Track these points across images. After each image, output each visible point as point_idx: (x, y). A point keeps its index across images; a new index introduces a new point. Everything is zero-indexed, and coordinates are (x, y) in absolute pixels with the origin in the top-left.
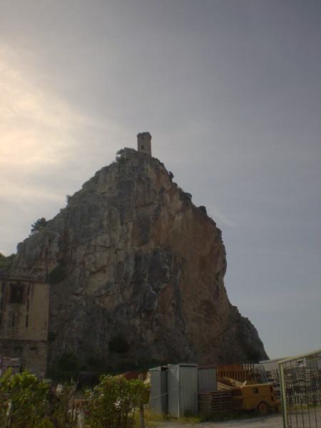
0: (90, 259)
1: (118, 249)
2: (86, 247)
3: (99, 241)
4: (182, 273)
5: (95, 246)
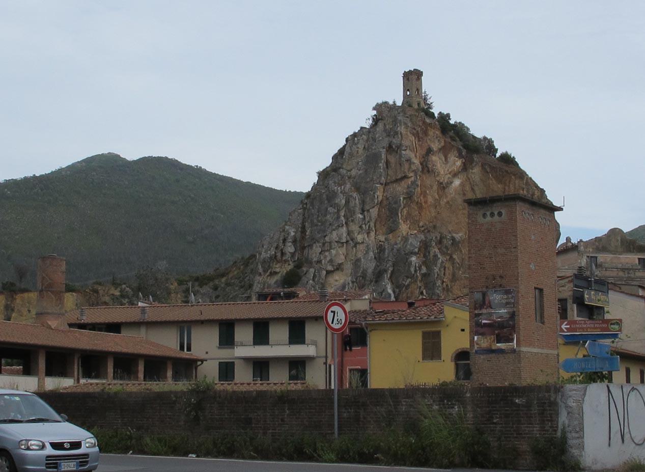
0: (325, 257)
1: (359, 243)
3: (334, 236)
4: (442, 161)
5: (330, 243)
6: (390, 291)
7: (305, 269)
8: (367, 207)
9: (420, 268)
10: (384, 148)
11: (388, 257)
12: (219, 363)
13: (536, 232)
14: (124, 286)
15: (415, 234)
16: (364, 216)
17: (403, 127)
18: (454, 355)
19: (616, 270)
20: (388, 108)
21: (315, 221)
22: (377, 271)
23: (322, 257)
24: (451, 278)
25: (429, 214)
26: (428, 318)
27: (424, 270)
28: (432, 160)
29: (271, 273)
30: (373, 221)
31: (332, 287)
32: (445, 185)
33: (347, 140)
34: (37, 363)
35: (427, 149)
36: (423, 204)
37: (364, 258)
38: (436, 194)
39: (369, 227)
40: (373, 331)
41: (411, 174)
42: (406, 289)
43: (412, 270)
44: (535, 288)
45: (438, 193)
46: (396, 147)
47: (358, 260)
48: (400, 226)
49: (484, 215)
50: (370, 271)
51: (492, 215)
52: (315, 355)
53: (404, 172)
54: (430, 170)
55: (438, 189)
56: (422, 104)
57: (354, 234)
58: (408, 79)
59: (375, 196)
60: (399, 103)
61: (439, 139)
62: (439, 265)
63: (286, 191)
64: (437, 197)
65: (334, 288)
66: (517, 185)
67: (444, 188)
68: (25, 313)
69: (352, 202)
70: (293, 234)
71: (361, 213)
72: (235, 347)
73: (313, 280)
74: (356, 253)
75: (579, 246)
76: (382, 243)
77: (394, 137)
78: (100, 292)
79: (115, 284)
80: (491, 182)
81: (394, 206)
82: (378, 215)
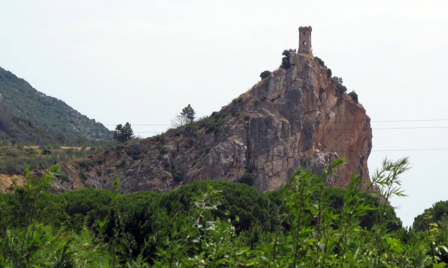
0: (268, 166)
1: (290, 157)
2: (265, 156)
5: (273, 156)
8: (294, 132)
17: (313, 73)
21: (258, 138)
29: (229, 175)
30: (298, 141)
31: (272, 188)
61: (326, 81)
69: (286, 127)
74: (288, 165)
81: (309, 131)
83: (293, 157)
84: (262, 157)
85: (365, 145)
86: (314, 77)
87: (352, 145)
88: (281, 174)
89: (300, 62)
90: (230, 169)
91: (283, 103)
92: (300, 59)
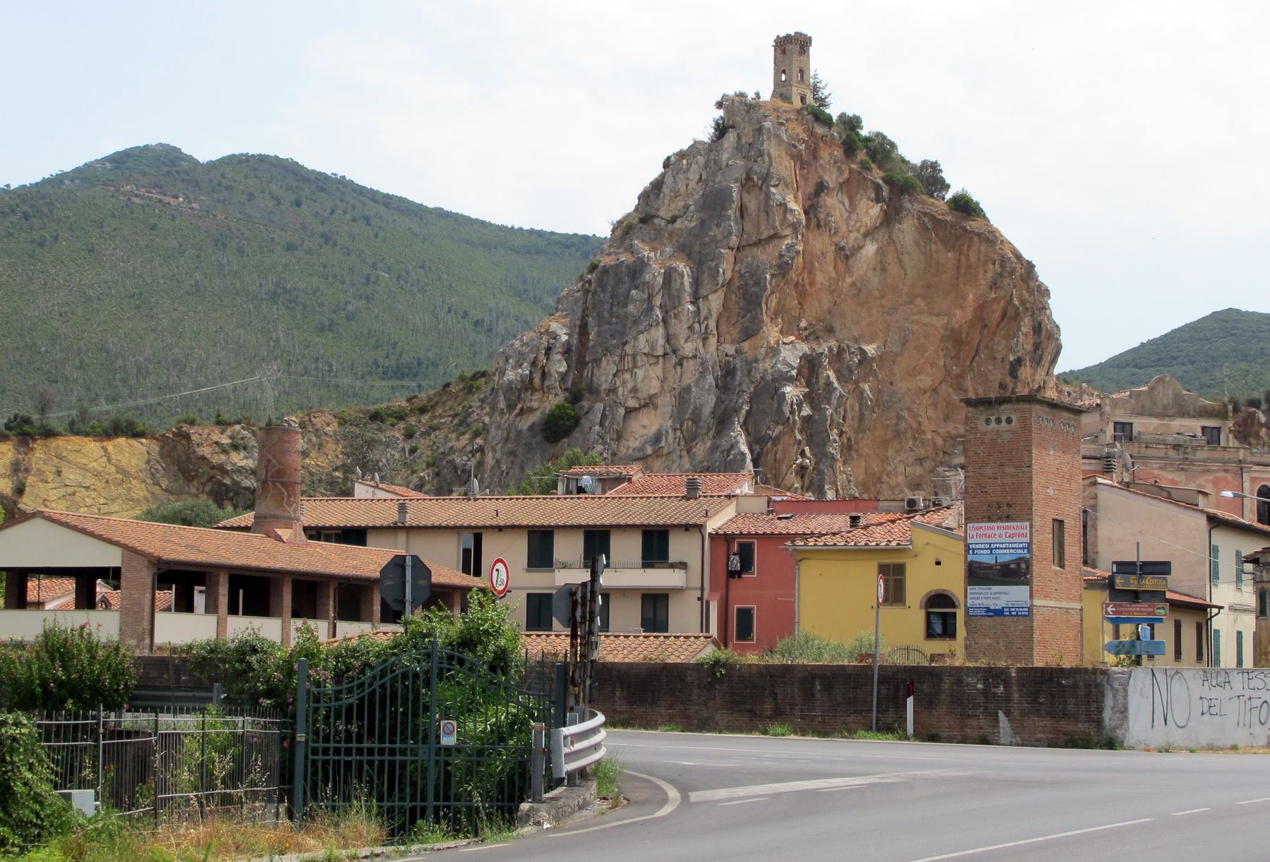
0: (624, 383)
1: (687, 358)
2: (617, 358)
5: (634, 356)
6: (744, 448)
7: (585, 404)
8: (703, 292)
9: (800, 405)
10: (736, 182)
11: (740, 384)
12: (528, 594)
13: (1056, 443)
14: (237, 427)
15: (792, 342)
16: (698, 308)
17: (773, 142)
18: (925, 600)
19: (1163, 447)
20: (746, 104)
21: (606, 315)
22: (719, 412)
23: (618, 383)
24: (856, 425)
25: (817, 305)
26: (887, 545)
27: (806, 411)
28: (825, 205)
29: (522, 409)
30: (715, 316)
31: (636, 439)
32: (848, 253)
33: (667, 164)
34: (281, 596)
35: (817, 184)
36: (808, 287)
37: (697, 386)
38: (832, 268)
39: (707, 328)
40: (804, 561)
41: (788, 231)
42: (775, 444)
43: (787, 410)
44: (1053, 520)
45: (835, 267)
46: (758, 179)
47: (687, 389)
48: (765, 328)
49: (988, 421)
50: (707, 410)
51: (999, 421)
52: (685, 586)
53: (774, 228)
54: (822, 223)
55: (835, 260)
56: (810, 100)
57: (679, 341)
58: (784, 52)
59: (718, 271)
60: (766, 96)
61: (839, 165)
62: (834, 402)
63: (513, 227)
64: (833, 274)
65: (639, 440)
66: (982, 255)
67: (847, 258)
68: (51, 476)
69: (676, 280)
70: (564, 338)
71: (691, 302)
72: (556, 570)
73: (601, 424)
74: (681, 376)
75: (1103, 405)
76: (731, 359)
77: (755, 161)
78: (193, 438)
79: (221, 423)
80: (933, 246)
82: (723, 306)
83: (695, 357)
84: (611, 359)
85: (1023, 328)
86: (777, 153)
87: (957, 326)
88: (659, 401)
89: (747, 118)
90: (523, 395)
91: (693, 224)
92: (747, 112)
